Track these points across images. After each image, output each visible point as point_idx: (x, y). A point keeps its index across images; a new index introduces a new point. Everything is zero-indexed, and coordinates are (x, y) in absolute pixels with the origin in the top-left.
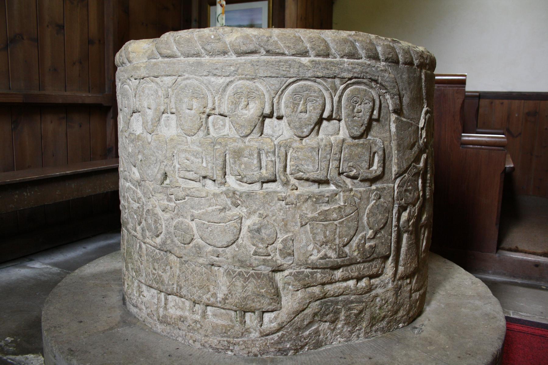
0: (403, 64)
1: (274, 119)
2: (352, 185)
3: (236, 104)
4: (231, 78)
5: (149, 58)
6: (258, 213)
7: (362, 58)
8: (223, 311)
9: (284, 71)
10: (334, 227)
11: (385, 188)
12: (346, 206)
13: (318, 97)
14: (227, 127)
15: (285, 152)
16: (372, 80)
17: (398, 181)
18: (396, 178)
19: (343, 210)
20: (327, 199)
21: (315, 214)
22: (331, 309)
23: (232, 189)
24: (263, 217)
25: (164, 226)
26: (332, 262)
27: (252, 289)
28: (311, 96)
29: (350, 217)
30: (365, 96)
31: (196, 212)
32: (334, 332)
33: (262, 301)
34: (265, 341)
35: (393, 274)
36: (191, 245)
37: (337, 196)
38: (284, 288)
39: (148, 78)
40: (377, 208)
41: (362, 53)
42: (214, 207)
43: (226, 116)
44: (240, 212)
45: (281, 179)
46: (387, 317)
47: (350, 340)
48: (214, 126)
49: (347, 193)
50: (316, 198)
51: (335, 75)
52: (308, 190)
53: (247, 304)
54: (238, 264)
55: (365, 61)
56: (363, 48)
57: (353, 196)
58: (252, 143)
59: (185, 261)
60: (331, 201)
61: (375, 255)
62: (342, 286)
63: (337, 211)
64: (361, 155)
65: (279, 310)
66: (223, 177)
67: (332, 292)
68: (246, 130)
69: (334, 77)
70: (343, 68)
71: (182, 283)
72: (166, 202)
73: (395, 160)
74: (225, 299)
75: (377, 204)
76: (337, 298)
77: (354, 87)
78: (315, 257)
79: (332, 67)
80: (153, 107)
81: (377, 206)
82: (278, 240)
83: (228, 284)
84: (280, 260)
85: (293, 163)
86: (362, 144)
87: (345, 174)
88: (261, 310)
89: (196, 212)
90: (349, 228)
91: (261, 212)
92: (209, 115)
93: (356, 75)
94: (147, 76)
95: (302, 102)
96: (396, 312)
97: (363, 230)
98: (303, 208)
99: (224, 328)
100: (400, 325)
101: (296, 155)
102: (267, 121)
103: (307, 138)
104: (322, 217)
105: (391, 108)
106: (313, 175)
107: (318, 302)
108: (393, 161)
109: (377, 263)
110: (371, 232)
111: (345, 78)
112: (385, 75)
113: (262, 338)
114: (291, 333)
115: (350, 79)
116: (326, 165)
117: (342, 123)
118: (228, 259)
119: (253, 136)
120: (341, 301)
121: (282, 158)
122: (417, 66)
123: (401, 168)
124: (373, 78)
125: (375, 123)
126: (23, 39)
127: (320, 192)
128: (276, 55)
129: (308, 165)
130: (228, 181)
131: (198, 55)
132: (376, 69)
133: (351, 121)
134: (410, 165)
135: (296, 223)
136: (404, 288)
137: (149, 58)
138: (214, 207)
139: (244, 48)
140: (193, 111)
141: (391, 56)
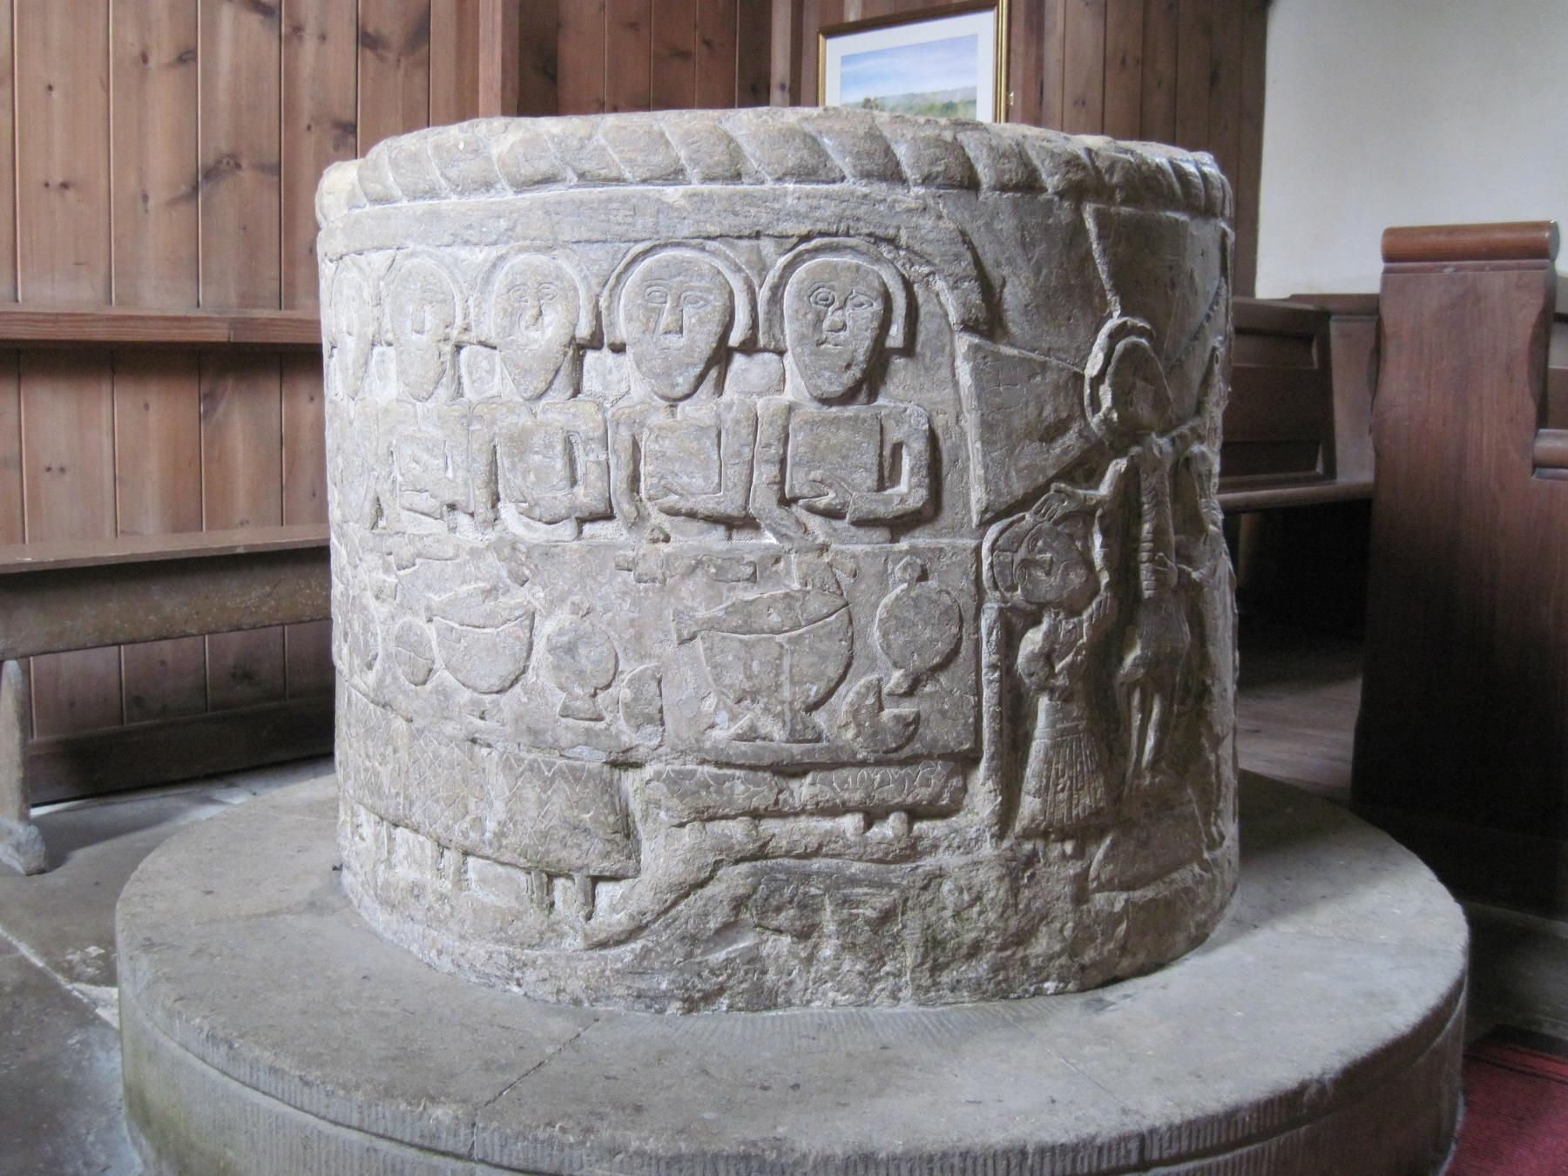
0: (994, 188)
1: (606, 350)
2: (828, 535)
3: (512, 315)
4: (502, 249)
5: (352, 206)
6: (569, 602)
7: (843, 179)
8: (500, 869)
9: (619, 224)
10: (775, 652)
11: (941, 550)
12: (808, 592)
13: (709, 291)
14: (498, 377)
15: (631, 439)
16: (878, 240)
17: (992, 532)
18: (984, 525)
19: (798, 604)
20: (749, 570)
21: (717, 611)
22: (787, 892)
23: (509, 538)
24: (581, 613)
25: (379, 638)
26: (775, 752)
27: (561, 810)
28: (691, 289)
29: (822, 627)
30: (854, 282)
31: (437, 599)
32: (813, 970)
33: (585, 847)
34: (599, 964)
35: (993, 812)
36: (428, 686)
37: (782, 564)
38: (645, 817)
40: (916, 606)
41: (844, 164)
42: (473, 586)
43: (495, 348)
44: (530, 598)
45: (621, 511)
46: (989, 949)
47: (867, 1003)
48: (470, 373)
49: (810, 557)
50: (715, 566)
51: (758, 228)
52: (696, 543)
53: (548, 852)
54: (525, 740)
55: (853, 187)
56: (844, 152)
57: (830, 565)
58: (550, 415)
59: (418, 730)
60: (762, 577)
61: (918, 745)
62: (816, 827)
63: (780, 606)
64: (850, 449)
65: (634, 877)
66: (489, 506)
67: (784, 843)
68: (535, 382)
69: (758, 235)
70: (780, 210)
71: (414, 792)
72: (382, 576)
73: (976, 470)
74: (500, 835)
75: (913, 594)
76: (805, 862)
77: (821, 259)
78: (721, 734)
79: (747, 208)
80: (355, 331)
81: (916, 600)
82: (621, 677)
83: (507, 793)
84: (628, 737)
85: (651, 468)
86: (849, 418)
87: (801, 502)
88: (585, 872)
89: (435, 599)
90: (824, 658)
91: (576, 599)
92: (459, 347)
93: (820, 226)
95: (668, 306)
96: (1022, 938)
97: (872, 667)
98: (684, 593)
99: (498, 916)
100: (1047, 985)
101: (657, 447)
102: (591, 357)
103: (688, 401)
104: (736, 621)
105: (953, 317)
106: (707, 503)
107: (744, 867)
108: (972, 472)
109: (932, 772)
110: (897, 674)
111: (787, 237)
112: (921, 221)
113: (590, 952)
114: (670, 948)
115: (806, 238)
116: (741, 475)
117: (789, 359)
118: (504, 725)
119: (554, 398)
120: (818, 873)
121: (623, 455)
122: (1056, 193)
123: (999, 494)
124: (880, 232)
125: (899, 362)
126: (238, 166)
127: (728, 551)
128: (603, 185)
129: (691, 475)
130: (503, 516)
131: (432, 193)
132: (891, 207)
133: (811, 354)
134: (1045, 487)
135: (666, 633)
136: (1048, 864)
137: (352, 206)
138: (473, 586)
139: (527, 171)
140: (425, 337)
141: (940, 169)
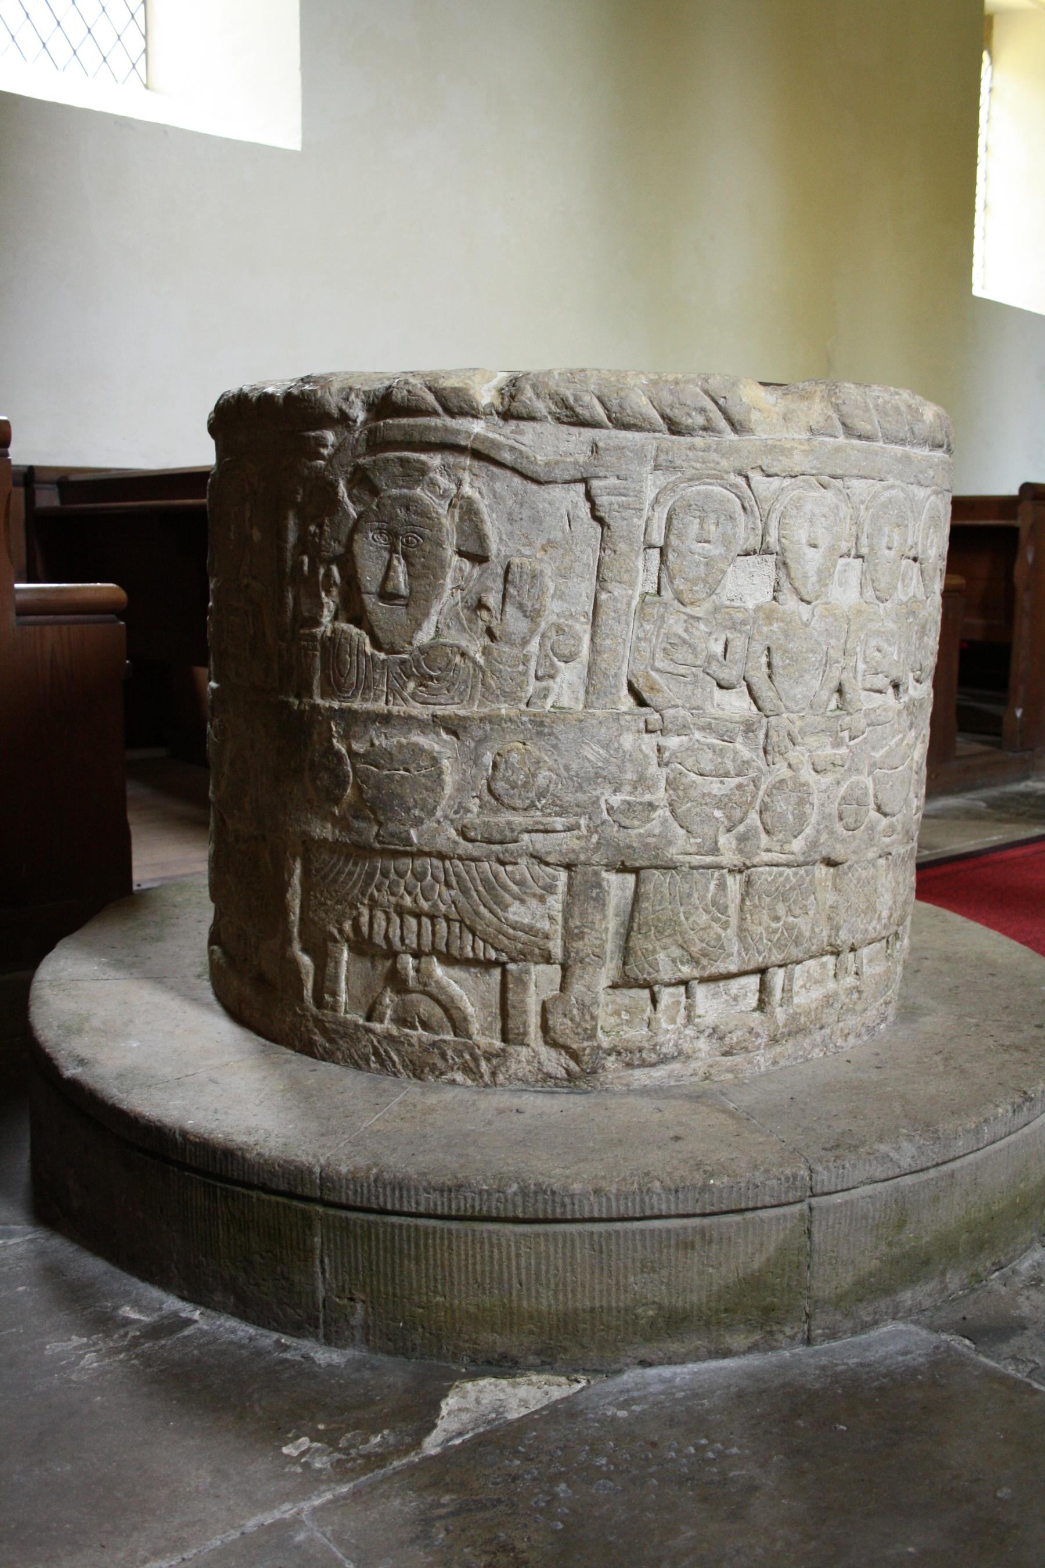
39: (812, 478)
72: (829, 751)
80: (824, 542)
94: (814, 472)
